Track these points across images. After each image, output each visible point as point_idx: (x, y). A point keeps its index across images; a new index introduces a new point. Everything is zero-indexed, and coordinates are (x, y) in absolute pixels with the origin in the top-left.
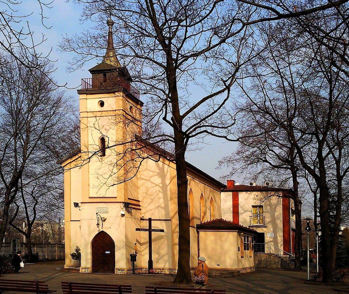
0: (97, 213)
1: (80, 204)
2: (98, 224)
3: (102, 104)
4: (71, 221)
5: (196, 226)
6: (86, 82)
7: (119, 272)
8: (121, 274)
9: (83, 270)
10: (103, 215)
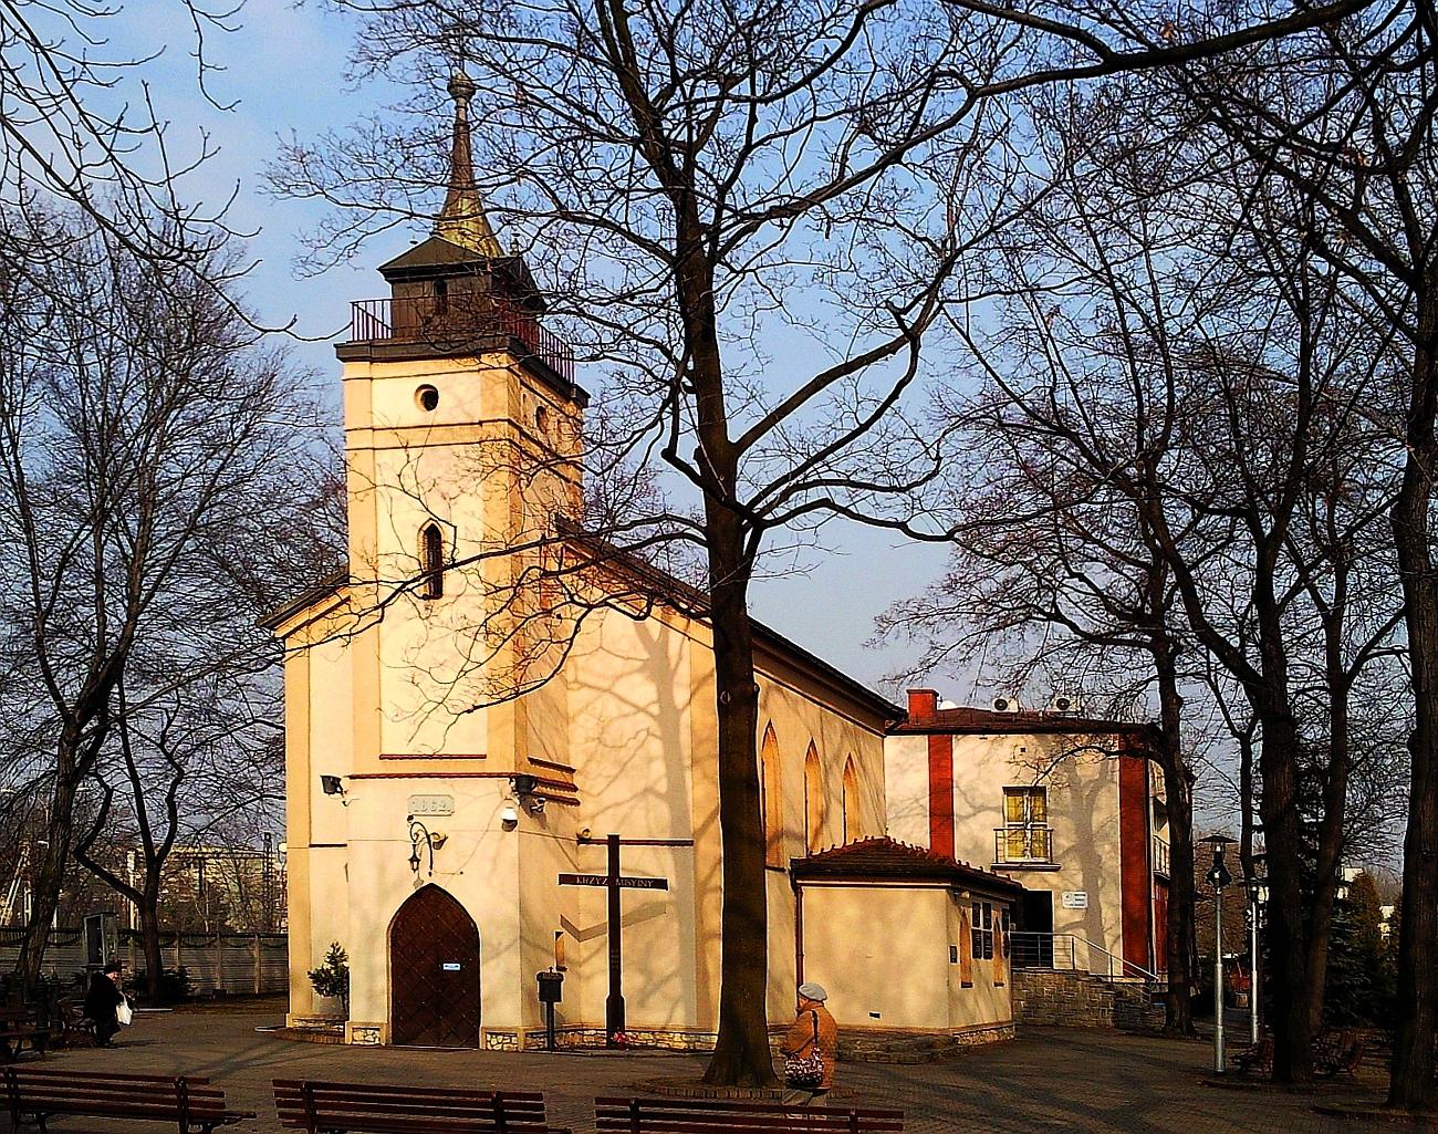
0: (410, 818)
1: (345, 783)
2: (414, 859)
3: (430, 398)
4: (311, 846)
5: (788, 867)
6: (368, 314)
7: (494, 1042)
8: (502, 1050)
9: (359, 1035)
10: (433, 825)
